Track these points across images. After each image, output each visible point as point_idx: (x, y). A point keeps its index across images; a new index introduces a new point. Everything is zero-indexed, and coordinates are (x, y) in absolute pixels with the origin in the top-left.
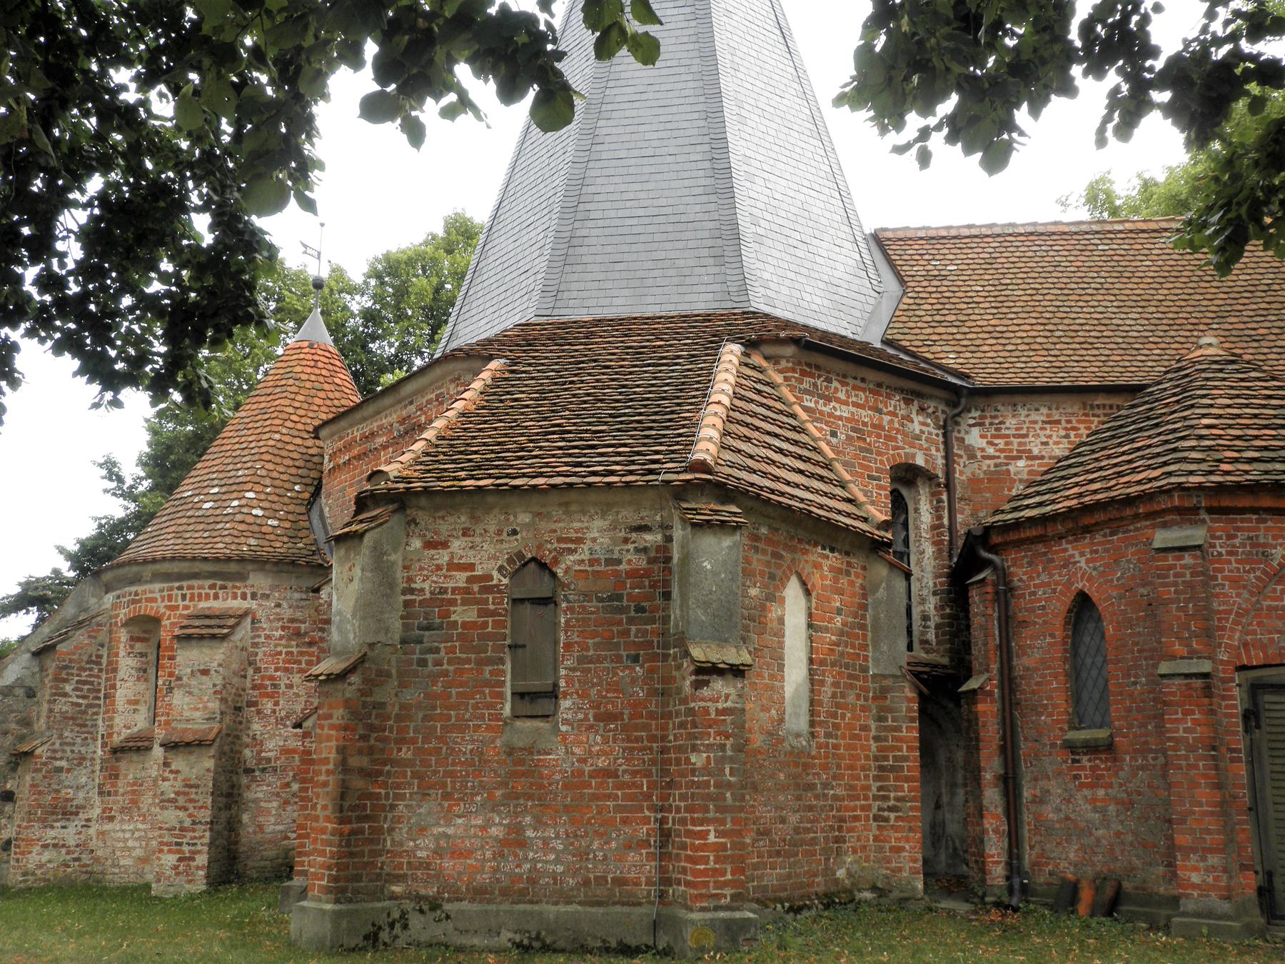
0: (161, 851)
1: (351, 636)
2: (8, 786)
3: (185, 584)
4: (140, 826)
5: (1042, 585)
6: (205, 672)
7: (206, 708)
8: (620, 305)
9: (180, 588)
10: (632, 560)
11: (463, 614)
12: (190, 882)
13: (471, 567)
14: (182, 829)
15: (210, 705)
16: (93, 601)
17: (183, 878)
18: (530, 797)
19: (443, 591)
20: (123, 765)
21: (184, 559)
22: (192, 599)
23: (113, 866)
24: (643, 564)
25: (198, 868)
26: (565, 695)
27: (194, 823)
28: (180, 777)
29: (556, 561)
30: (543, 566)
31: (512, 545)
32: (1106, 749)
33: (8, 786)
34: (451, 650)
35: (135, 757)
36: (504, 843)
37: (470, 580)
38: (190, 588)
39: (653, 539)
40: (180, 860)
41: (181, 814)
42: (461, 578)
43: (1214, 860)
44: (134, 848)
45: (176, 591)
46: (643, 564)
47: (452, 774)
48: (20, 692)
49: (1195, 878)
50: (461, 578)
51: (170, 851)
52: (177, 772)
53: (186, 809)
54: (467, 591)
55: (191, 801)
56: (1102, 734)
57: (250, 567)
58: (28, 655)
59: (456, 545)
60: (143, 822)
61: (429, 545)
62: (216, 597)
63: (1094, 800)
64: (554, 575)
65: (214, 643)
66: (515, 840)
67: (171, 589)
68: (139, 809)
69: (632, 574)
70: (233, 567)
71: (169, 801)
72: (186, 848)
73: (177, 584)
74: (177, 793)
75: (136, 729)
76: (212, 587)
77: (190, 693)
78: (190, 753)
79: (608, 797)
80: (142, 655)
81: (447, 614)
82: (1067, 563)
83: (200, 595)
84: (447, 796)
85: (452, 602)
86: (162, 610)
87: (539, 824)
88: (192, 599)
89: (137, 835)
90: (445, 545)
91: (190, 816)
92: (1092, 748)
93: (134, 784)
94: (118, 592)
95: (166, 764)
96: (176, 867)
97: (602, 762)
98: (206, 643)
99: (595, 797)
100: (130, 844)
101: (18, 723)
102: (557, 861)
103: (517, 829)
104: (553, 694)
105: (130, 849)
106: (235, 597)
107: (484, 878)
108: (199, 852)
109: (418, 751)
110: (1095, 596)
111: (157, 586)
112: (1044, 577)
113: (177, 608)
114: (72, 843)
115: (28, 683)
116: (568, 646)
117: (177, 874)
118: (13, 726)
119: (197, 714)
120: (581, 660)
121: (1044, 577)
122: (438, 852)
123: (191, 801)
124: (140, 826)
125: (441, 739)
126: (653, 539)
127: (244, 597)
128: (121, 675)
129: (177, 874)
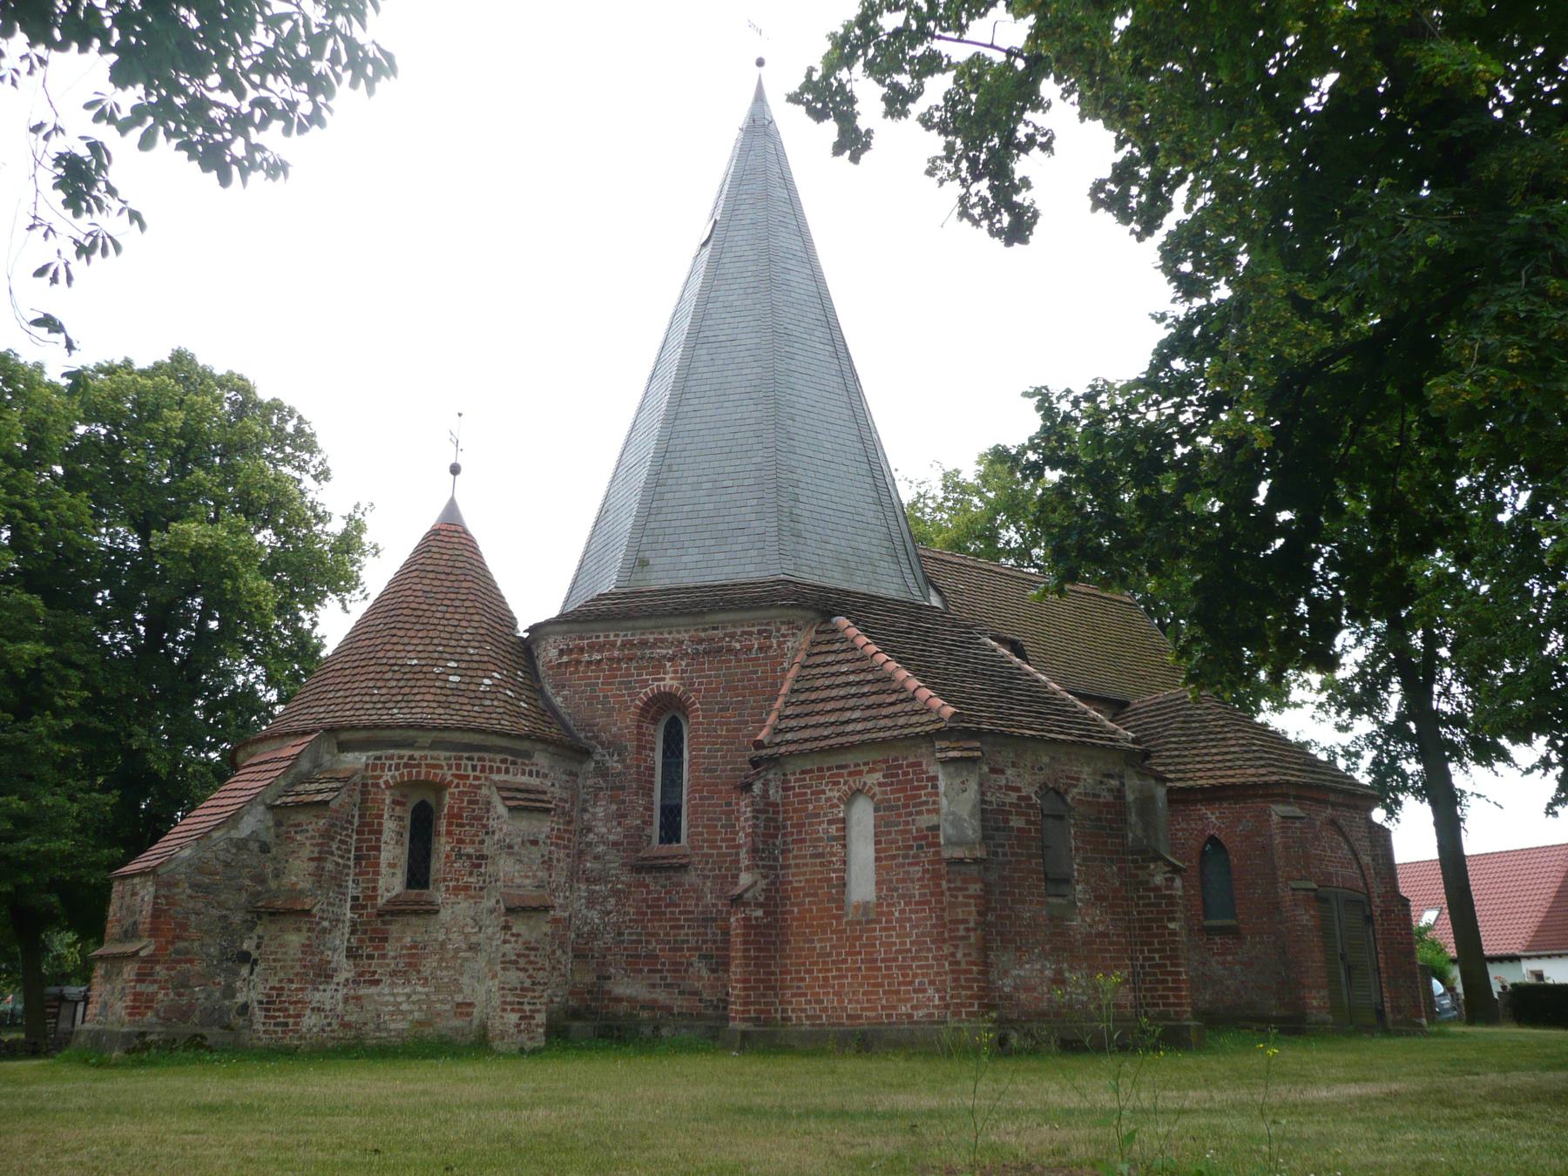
0: (504, 1010)
1: (970, 832)
2: (245, 946)
3: (476, 755)
4: (420, 989)
5: (1183, 830)
6: (535, 843)
7: (535, 876)
8: (863, 589)
9: (469, 759)
10: (1107, 797)
11: (1016, 822)
12: (531, 1039)
13: (1018, 789)
14: (523, 989)
15: (539, 874)
16: (327, 757)
17: (525, 1036)
18: (1065, 950)
19: (1004, 804)
20: (395, 929)
21: (483, 731)
22: (483, 770)
23: (378, 1028)
24: (1111, 799)
25: (538, 1026)
26: (1078, 882)
27: (534, 983)
28: (521, 940)
29: (1066, 792)
30: (1057, 792)
31: (1040, 777)
32: (1234, 932)
33: (245, 946)
34: (1012, 846)
35: (414, 920)
36: (1054, 981)
37: (1020, 798)
38: (480, 759)
39: (1114, 783)
40: (521, 1018)
41: (521, 974)
42: (1013, 797)
43: (1324, 993)
44: (412, 1012)
45: (464, 762)
46: (1111, 799)
47: (1018, 933)
48: (254, 846)
49: (1315, 1003)
50: (1013, 797)
51: (513, 1010)
52: (518, 935)
53: (526, 970)
54: (1018, 806)
55: (531, 962)
56: (1232, 922)
57: (539, 746)
58: (262, 808)
59: (1009, 772)
60: (424, 985)
61: (993, 770)
62: (507, 771)
63: (1223, 963)
64: (1064, 801)
65: (541, 816)
66: (1059, 980)
67: (460, 758)
68: (419, 972)
69: (1106, 805)
70: (526, 745)
71: (511, 962)
72: (527, 1007)
73: (466, 755)
74: (518, 955)
75: (394, 893)
76: (504, 761)
77: (520, 861)
78: (530, 918)
79: (1107, 950)
80: (401, 819)
81: (1006, 821)
82: (1202, 818)
83: (491, 768)
84: (1018, 949)
85: (1010, 813)
86: (449, 778)
87: (1072, 969)
88: (483, 770)
89: (414, 998)
90: (1002, 772)
91: (530, 977)
92: (1223, 931)
93: (411, 948)
94: (378, 753)
95: (506, 927)
96: (518, 1025)
97: (1101, 928)
98: (536, 815)
99: (1101, 951)
100: (404, 1007)
101: (252, 878)
102: (1084, 993)
103: (1059, 972)
104: (1066, 881)
105: (402, 1013)
106: (523, 773)
107: (1044, 1005)
108: (539, 1011)
109: (999, 917)
110: (1221, 837)
111: (443, 754)
112: (1184, 825)
113: (467, 777)
114: (328, 1007)
115: (264, 836)
116: (1077, 849)
117: (520, 1032)
118: (248, 882)
119: (527, 881)
120: (1084, 859)
121: (1184, 825)
122: (1016, 988)
123: (531, 962)
124: (420, 989)
125: (1011, 909)
126: (1114, 783)
127: (531, 774)
128: (385, 837)
129: (520, 1032)
